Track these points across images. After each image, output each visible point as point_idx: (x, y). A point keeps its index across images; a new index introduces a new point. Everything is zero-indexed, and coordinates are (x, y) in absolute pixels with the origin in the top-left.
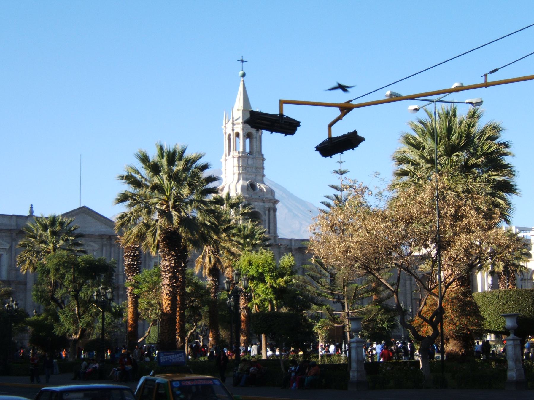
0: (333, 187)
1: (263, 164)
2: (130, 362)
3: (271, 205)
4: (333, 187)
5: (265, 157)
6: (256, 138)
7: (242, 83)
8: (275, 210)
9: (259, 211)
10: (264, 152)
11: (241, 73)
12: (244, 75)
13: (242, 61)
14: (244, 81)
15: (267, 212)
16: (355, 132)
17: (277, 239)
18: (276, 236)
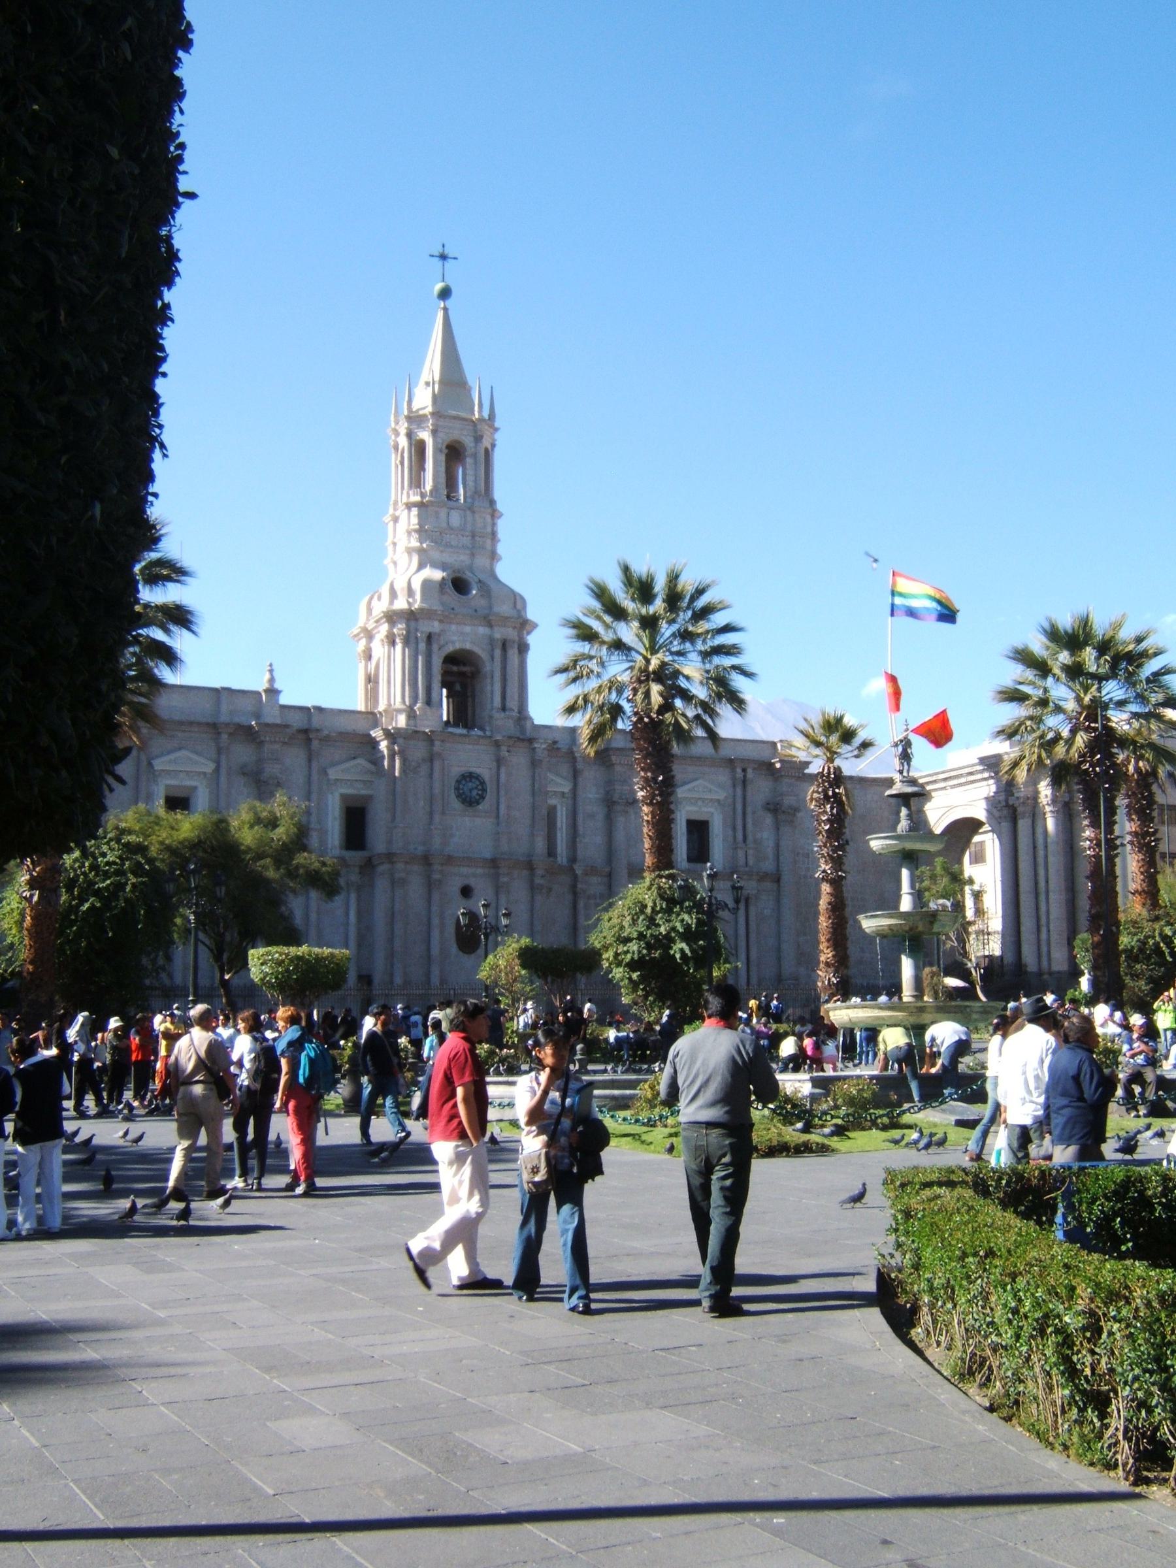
0: (806, 720)
1: (494, 525)
2: (575, 1157)
3: (511, 633)
4: (806, 720)
5: (500, 506)
6: (475, 456)
7: (440, 314)
8: (523, 648)
9: (477, 650)
10: (498, 494)
11: (439, 286)
12: (445, 294)
13: (443, 257)
14: (445, 309)
15: (498, 652)
16: (601, 1172)
17: (528, 725)
18: (522, 715)
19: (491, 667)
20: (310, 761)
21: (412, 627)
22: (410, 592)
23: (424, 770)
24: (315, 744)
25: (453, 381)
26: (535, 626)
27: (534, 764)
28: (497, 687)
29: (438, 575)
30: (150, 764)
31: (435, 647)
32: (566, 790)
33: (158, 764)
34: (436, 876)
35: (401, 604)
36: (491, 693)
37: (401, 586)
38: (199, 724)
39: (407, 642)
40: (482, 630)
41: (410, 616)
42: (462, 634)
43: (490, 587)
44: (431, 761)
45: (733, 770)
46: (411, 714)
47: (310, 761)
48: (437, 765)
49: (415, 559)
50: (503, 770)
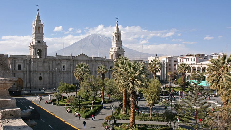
8: (46, 49)
12: (117, 22)
13: (38, 6)
14: (38, 12)
15: (43, 49)
19: (43, 51)
21: (34, 47)
22: (116, 49)
25: (39, 20)
28: (43, 53)
29: (37, 41)
32: (66, 63)
33: (17, 62)
34: (37, 73)
35: (115, 50)
36: (43, 53)
37: (115, 48)
38: (85, 60)
39: (33, 48)
41: (34, 46)
43: (122, 48)
46: (34, 56)
49: (116, 46)
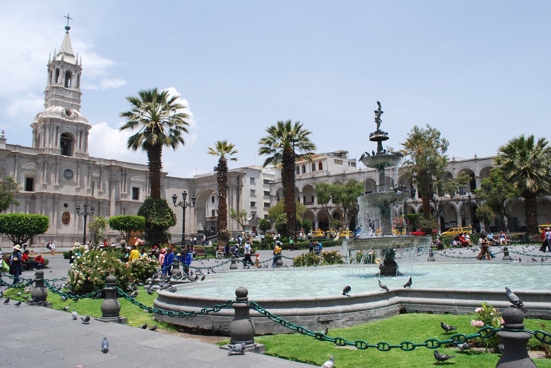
8: (87, 134)
13: (68, 18)
20: (15, 162)
23: (54, 167)
24: (17, 158)
26: (31, 126)
27: (89, 168)
30: (130, 178)
31: (59, 130)
33: (132, 179)
40: (76, 127)
42: (68, 128)
44: (56, 165)
45: (146, 174)
47: (15, 162)
48: (58, 166)
50: (79, 169)
